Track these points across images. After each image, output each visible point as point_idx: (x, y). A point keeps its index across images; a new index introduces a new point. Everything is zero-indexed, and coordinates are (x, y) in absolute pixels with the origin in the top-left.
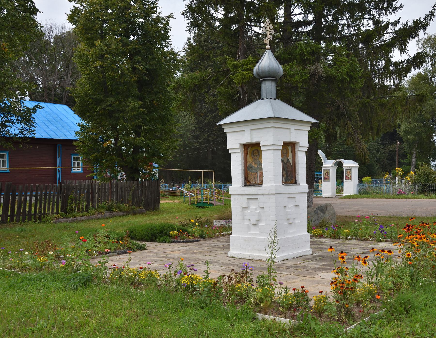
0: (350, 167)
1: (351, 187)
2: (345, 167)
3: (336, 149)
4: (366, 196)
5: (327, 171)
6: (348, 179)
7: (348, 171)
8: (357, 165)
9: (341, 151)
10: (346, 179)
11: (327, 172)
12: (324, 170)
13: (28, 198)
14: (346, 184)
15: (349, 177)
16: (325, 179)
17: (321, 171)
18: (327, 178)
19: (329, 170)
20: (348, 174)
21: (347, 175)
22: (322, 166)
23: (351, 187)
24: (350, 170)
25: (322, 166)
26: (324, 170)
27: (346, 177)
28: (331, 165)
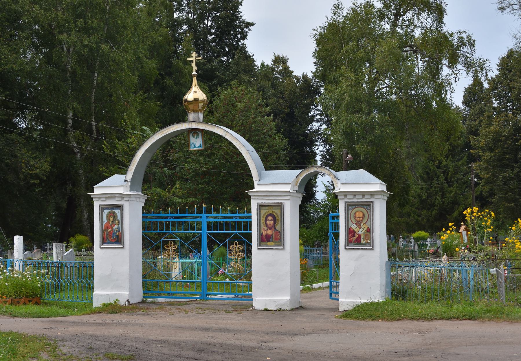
0: (363, 194)
1: (363, 273)
2: (346, 194)
3: (195, 166)
4: (439, 307)
5: (270, 211)
6: (358, 242)
7: (359, 212)
8: (377, 185)
9: (204, 173)
10: (349, 242)
11: (273, 214)
12: (261, 206)
13: (77, 271)
14: (348, 259)
15: (361, 232)
16: (264, 239)
17: (249, 211)
18: (273, 237)
19: (280, 206)
20: (358, 224)
21: (354, 227)
22: (250, 192)
23: (363, 273)
24: (362, 205)
25: (250, 192)
26: (261, 206)
27: (350, 233)
28: (288, 188)
